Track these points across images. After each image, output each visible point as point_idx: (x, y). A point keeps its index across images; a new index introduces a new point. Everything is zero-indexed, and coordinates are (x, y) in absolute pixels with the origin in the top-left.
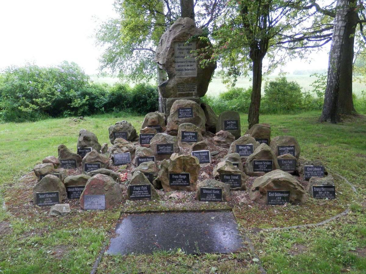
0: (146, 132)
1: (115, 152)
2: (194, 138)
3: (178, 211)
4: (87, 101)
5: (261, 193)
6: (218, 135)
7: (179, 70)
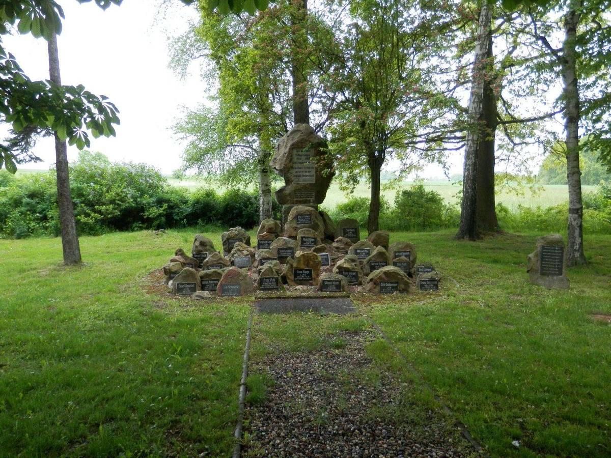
1: (235, 255)
3: (304, 297)
4: (164, 210)
5: (375, 284)
6: (337, 242)
7: (297, 176)
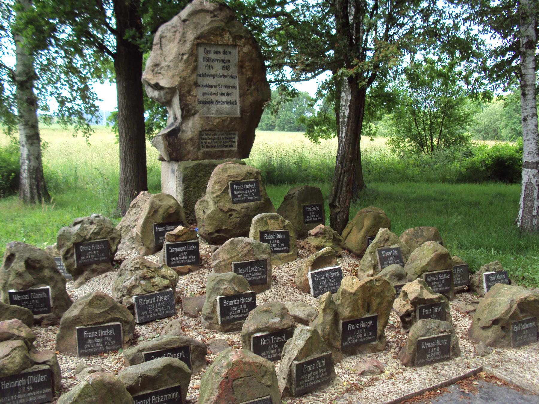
0: (181, 239)
2: (283, 245)
5: (503, 328)
6: (316, 235)
7: (205, 103)
